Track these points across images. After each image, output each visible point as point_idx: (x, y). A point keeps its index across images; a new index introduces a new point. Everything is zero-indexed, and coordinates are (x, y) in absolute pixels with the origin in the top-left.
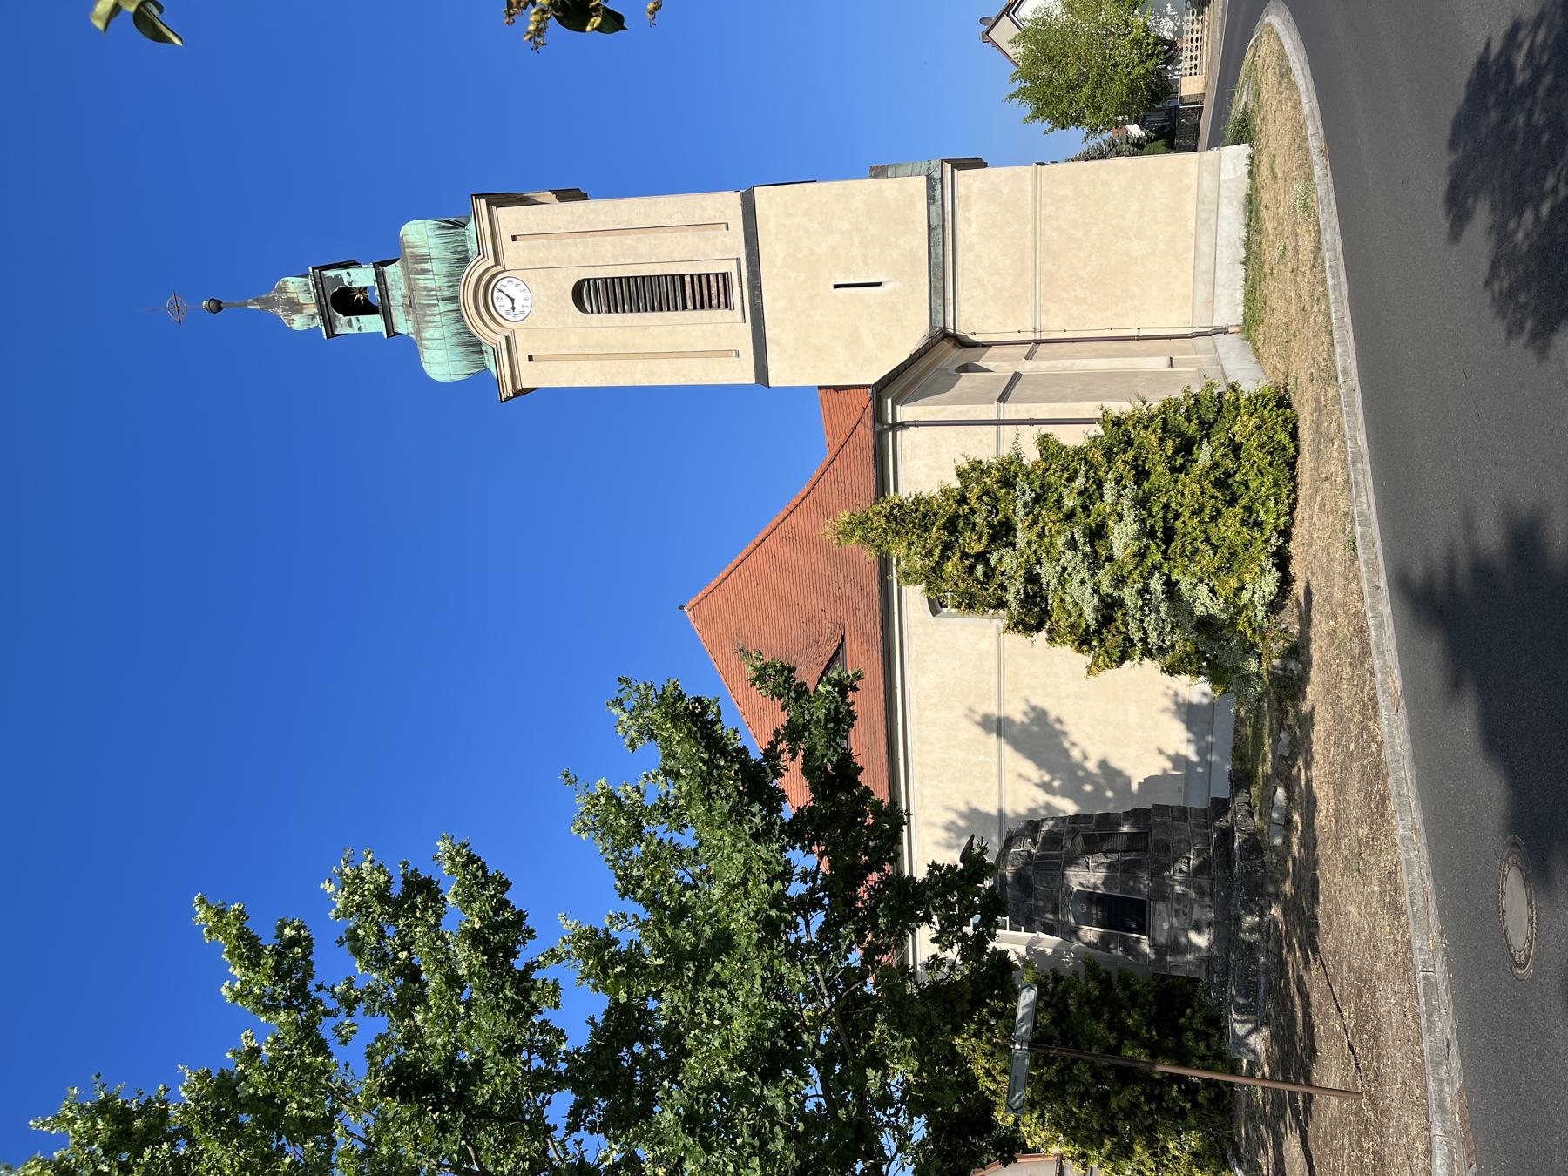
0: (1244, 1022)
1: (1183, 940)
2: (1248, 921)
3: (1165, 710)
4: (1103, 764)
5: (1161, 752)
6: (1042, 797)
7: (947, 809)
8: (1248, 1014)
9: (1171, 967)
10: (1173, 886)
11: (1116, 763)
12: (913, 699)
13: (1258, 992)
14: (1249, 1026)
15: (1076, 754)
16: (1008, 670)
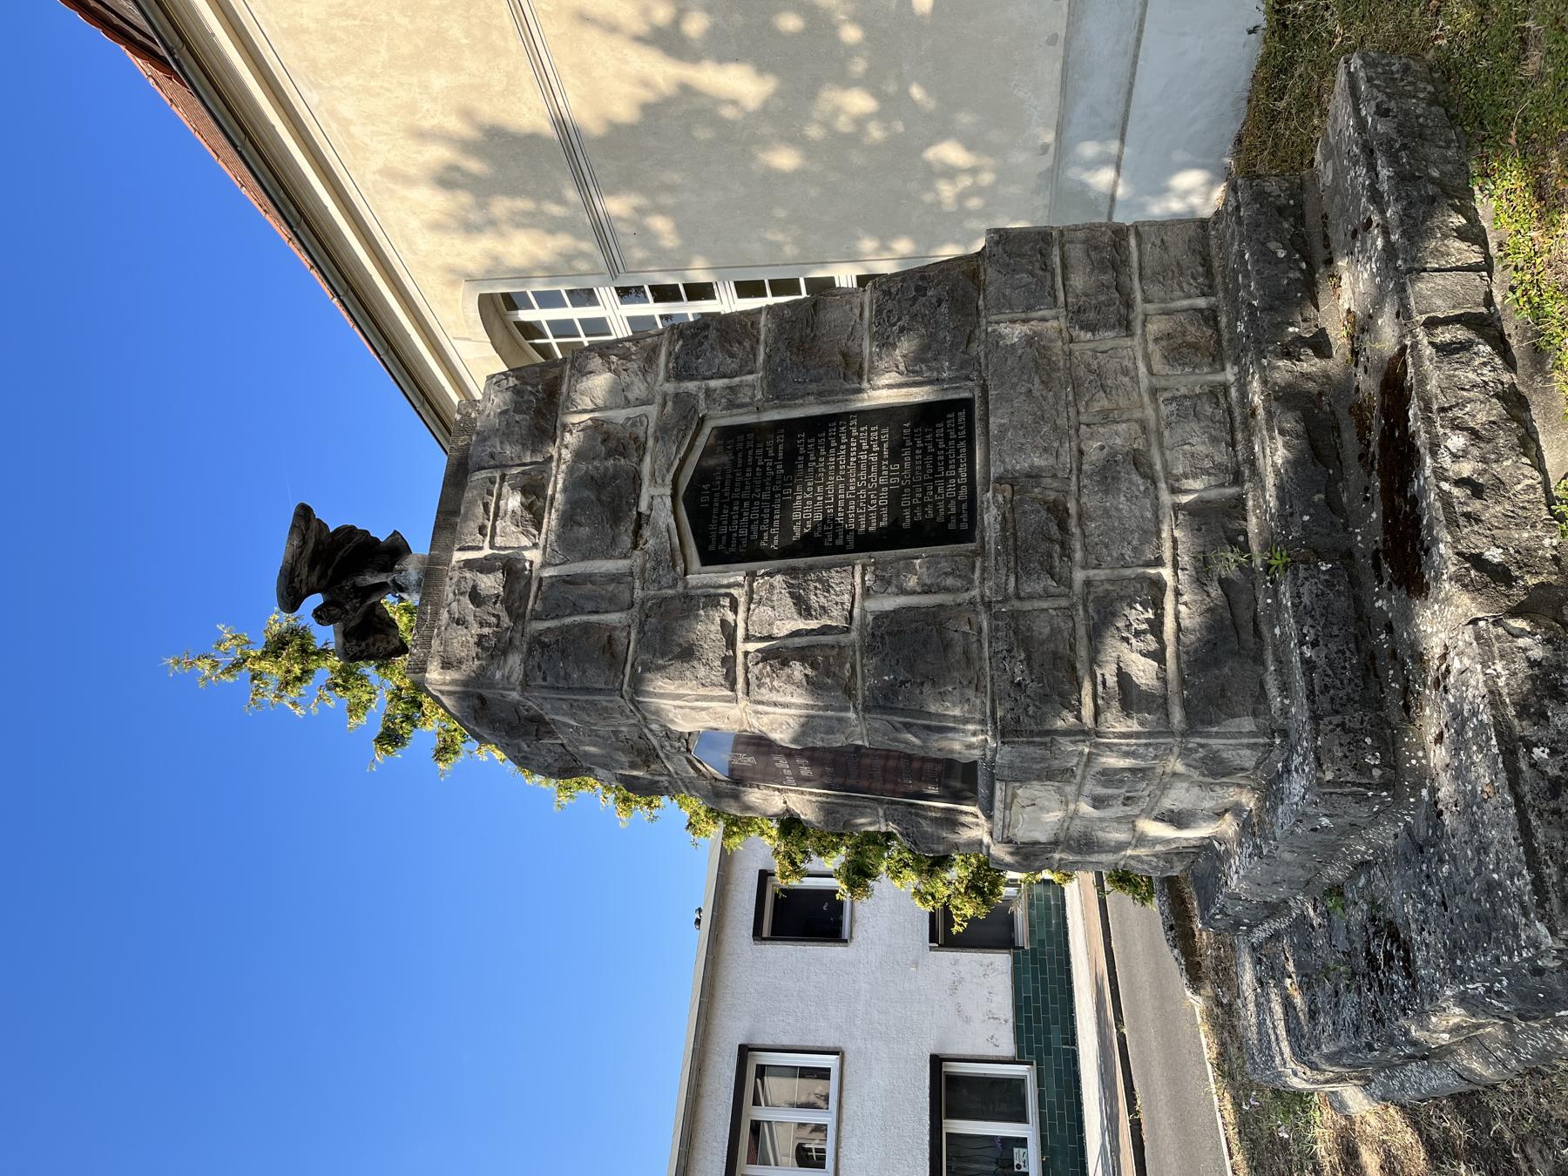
6: (664, 72)
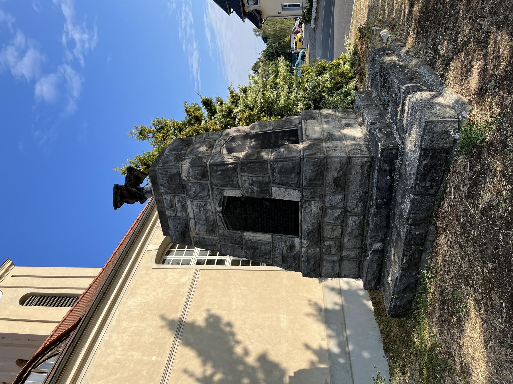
3: (308, 315)
4: (263, 358)
5: (307, 347)
11: (274, 356)
12: (117, 313)
15: (239, 350)
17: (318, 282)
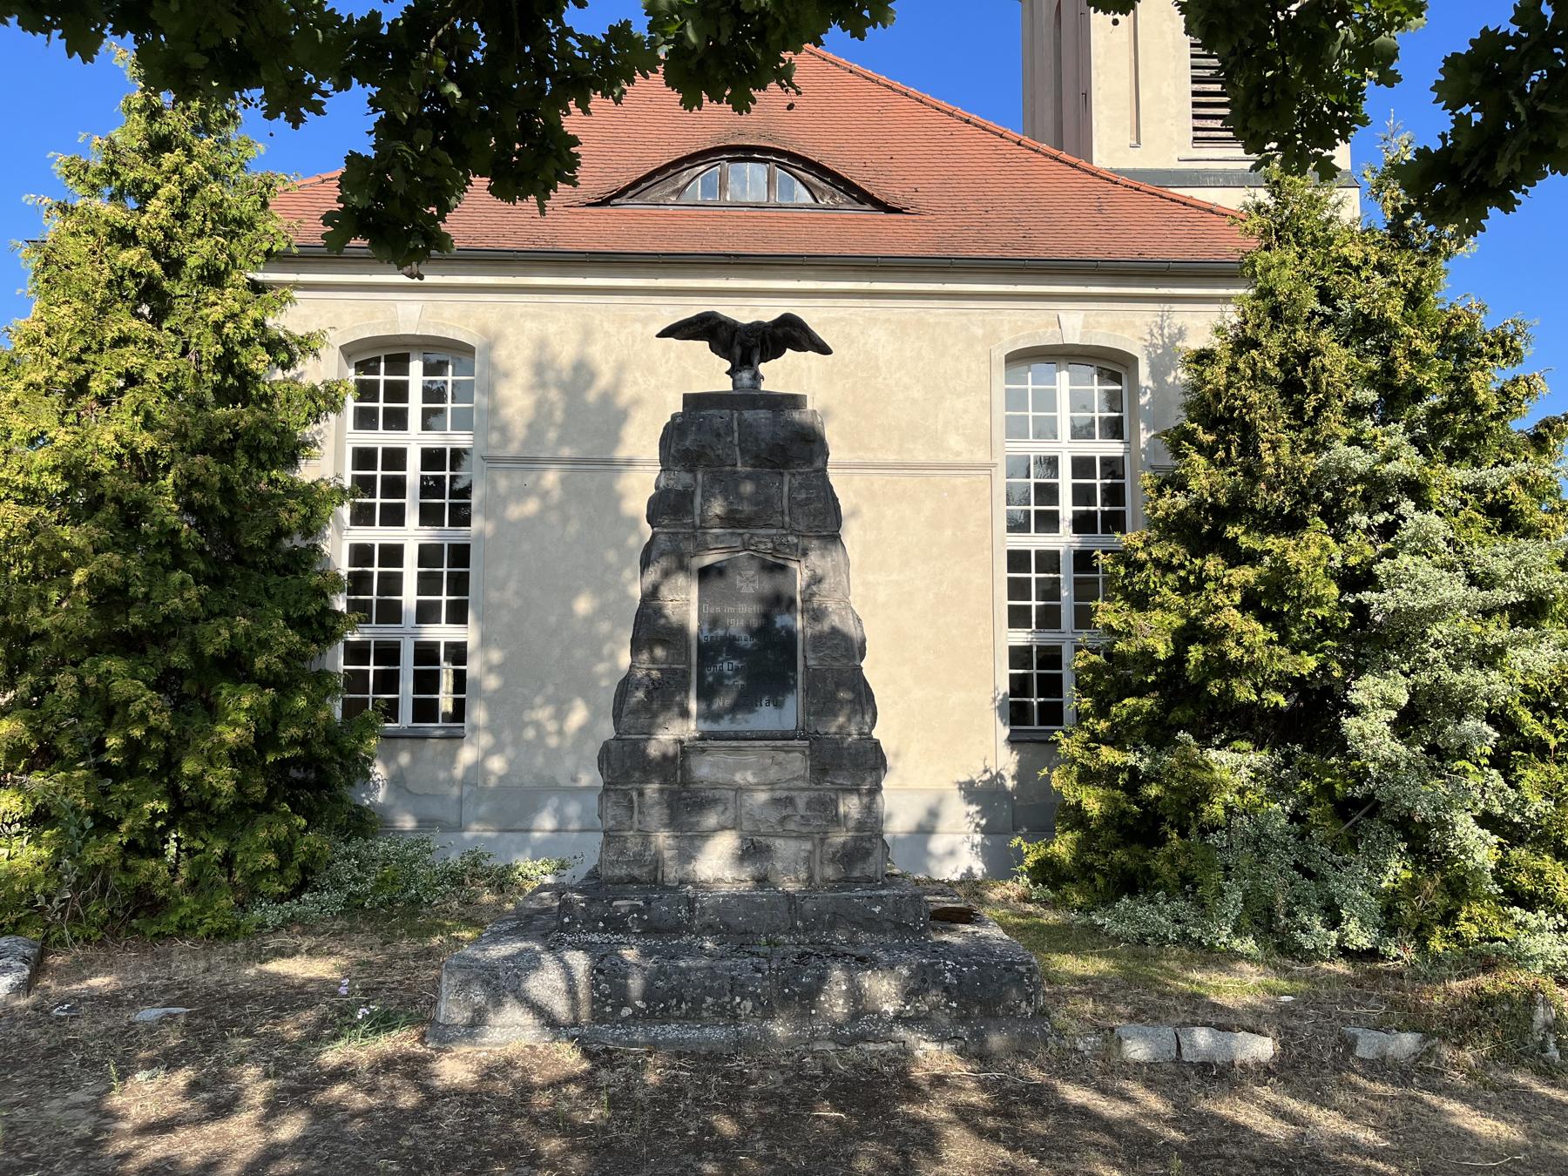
0: (572, 992)
1: (711, 820)
2: (884, 990)
7: (621, 368)
8: (594, 1001)
9: (626, 794)
10: (854, 790)
12: (842, 313)
13: (664, 1021)
14: (560, 1007)
16: (907, 482)
17: (962, 780)
